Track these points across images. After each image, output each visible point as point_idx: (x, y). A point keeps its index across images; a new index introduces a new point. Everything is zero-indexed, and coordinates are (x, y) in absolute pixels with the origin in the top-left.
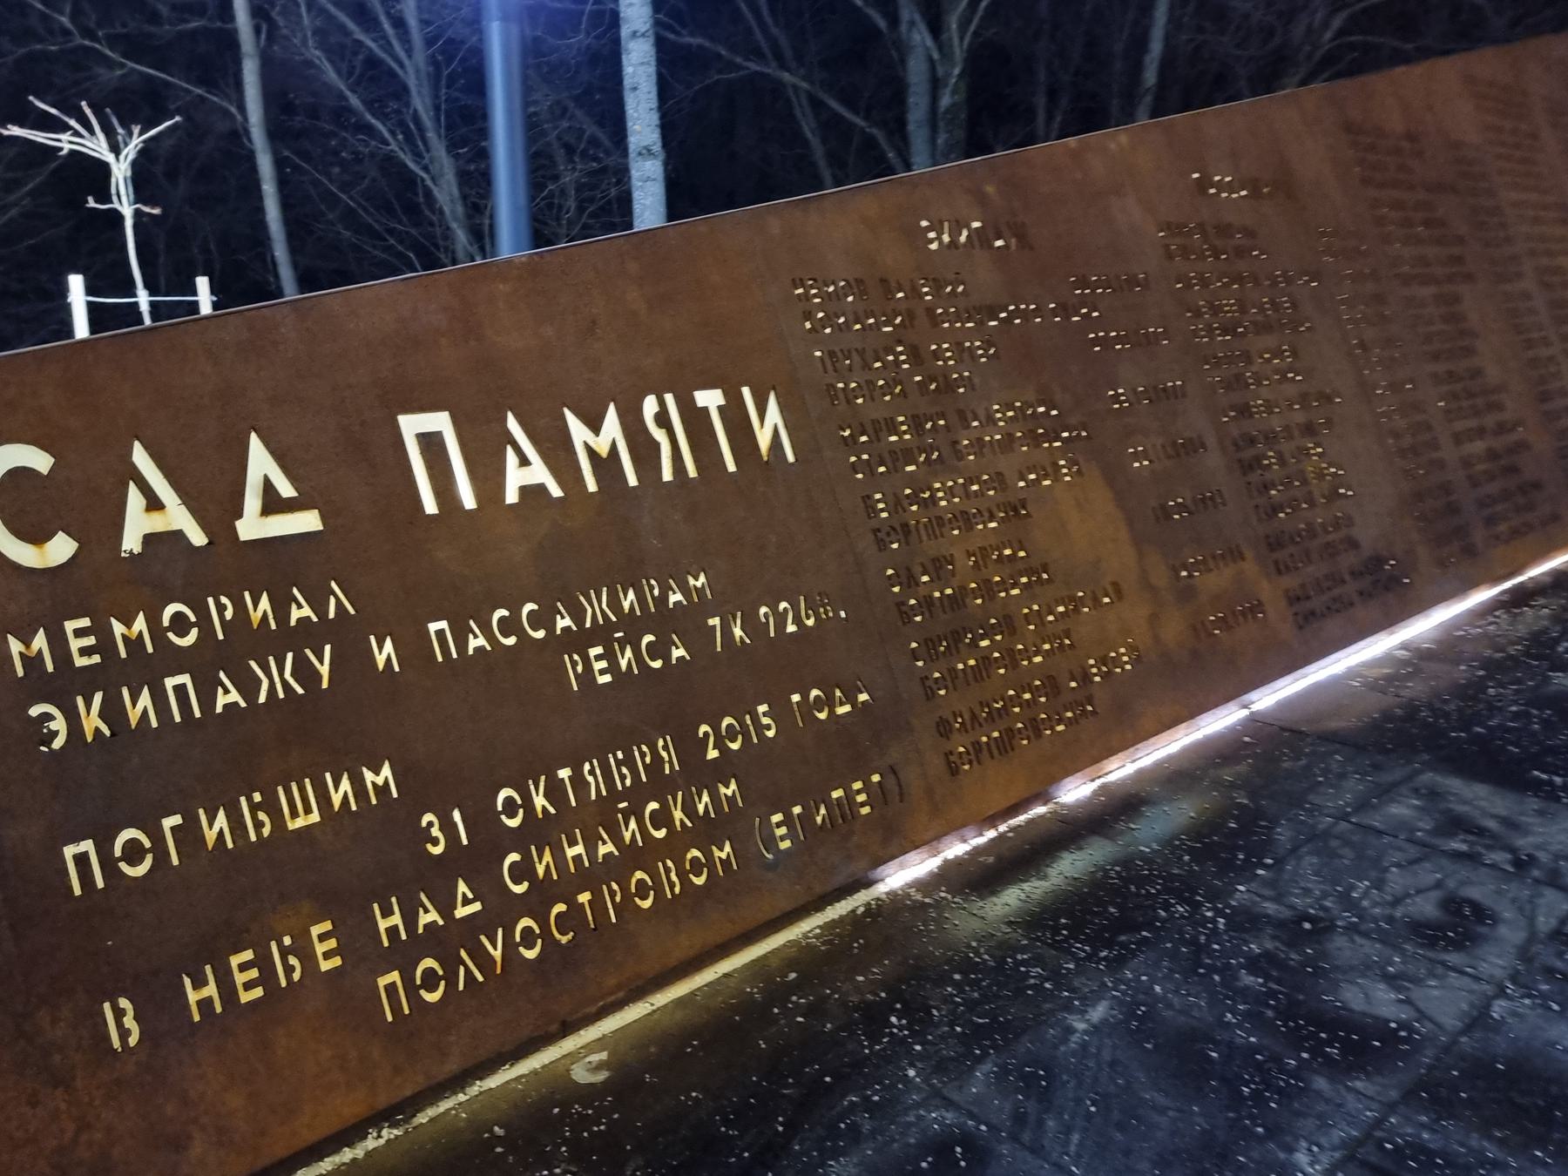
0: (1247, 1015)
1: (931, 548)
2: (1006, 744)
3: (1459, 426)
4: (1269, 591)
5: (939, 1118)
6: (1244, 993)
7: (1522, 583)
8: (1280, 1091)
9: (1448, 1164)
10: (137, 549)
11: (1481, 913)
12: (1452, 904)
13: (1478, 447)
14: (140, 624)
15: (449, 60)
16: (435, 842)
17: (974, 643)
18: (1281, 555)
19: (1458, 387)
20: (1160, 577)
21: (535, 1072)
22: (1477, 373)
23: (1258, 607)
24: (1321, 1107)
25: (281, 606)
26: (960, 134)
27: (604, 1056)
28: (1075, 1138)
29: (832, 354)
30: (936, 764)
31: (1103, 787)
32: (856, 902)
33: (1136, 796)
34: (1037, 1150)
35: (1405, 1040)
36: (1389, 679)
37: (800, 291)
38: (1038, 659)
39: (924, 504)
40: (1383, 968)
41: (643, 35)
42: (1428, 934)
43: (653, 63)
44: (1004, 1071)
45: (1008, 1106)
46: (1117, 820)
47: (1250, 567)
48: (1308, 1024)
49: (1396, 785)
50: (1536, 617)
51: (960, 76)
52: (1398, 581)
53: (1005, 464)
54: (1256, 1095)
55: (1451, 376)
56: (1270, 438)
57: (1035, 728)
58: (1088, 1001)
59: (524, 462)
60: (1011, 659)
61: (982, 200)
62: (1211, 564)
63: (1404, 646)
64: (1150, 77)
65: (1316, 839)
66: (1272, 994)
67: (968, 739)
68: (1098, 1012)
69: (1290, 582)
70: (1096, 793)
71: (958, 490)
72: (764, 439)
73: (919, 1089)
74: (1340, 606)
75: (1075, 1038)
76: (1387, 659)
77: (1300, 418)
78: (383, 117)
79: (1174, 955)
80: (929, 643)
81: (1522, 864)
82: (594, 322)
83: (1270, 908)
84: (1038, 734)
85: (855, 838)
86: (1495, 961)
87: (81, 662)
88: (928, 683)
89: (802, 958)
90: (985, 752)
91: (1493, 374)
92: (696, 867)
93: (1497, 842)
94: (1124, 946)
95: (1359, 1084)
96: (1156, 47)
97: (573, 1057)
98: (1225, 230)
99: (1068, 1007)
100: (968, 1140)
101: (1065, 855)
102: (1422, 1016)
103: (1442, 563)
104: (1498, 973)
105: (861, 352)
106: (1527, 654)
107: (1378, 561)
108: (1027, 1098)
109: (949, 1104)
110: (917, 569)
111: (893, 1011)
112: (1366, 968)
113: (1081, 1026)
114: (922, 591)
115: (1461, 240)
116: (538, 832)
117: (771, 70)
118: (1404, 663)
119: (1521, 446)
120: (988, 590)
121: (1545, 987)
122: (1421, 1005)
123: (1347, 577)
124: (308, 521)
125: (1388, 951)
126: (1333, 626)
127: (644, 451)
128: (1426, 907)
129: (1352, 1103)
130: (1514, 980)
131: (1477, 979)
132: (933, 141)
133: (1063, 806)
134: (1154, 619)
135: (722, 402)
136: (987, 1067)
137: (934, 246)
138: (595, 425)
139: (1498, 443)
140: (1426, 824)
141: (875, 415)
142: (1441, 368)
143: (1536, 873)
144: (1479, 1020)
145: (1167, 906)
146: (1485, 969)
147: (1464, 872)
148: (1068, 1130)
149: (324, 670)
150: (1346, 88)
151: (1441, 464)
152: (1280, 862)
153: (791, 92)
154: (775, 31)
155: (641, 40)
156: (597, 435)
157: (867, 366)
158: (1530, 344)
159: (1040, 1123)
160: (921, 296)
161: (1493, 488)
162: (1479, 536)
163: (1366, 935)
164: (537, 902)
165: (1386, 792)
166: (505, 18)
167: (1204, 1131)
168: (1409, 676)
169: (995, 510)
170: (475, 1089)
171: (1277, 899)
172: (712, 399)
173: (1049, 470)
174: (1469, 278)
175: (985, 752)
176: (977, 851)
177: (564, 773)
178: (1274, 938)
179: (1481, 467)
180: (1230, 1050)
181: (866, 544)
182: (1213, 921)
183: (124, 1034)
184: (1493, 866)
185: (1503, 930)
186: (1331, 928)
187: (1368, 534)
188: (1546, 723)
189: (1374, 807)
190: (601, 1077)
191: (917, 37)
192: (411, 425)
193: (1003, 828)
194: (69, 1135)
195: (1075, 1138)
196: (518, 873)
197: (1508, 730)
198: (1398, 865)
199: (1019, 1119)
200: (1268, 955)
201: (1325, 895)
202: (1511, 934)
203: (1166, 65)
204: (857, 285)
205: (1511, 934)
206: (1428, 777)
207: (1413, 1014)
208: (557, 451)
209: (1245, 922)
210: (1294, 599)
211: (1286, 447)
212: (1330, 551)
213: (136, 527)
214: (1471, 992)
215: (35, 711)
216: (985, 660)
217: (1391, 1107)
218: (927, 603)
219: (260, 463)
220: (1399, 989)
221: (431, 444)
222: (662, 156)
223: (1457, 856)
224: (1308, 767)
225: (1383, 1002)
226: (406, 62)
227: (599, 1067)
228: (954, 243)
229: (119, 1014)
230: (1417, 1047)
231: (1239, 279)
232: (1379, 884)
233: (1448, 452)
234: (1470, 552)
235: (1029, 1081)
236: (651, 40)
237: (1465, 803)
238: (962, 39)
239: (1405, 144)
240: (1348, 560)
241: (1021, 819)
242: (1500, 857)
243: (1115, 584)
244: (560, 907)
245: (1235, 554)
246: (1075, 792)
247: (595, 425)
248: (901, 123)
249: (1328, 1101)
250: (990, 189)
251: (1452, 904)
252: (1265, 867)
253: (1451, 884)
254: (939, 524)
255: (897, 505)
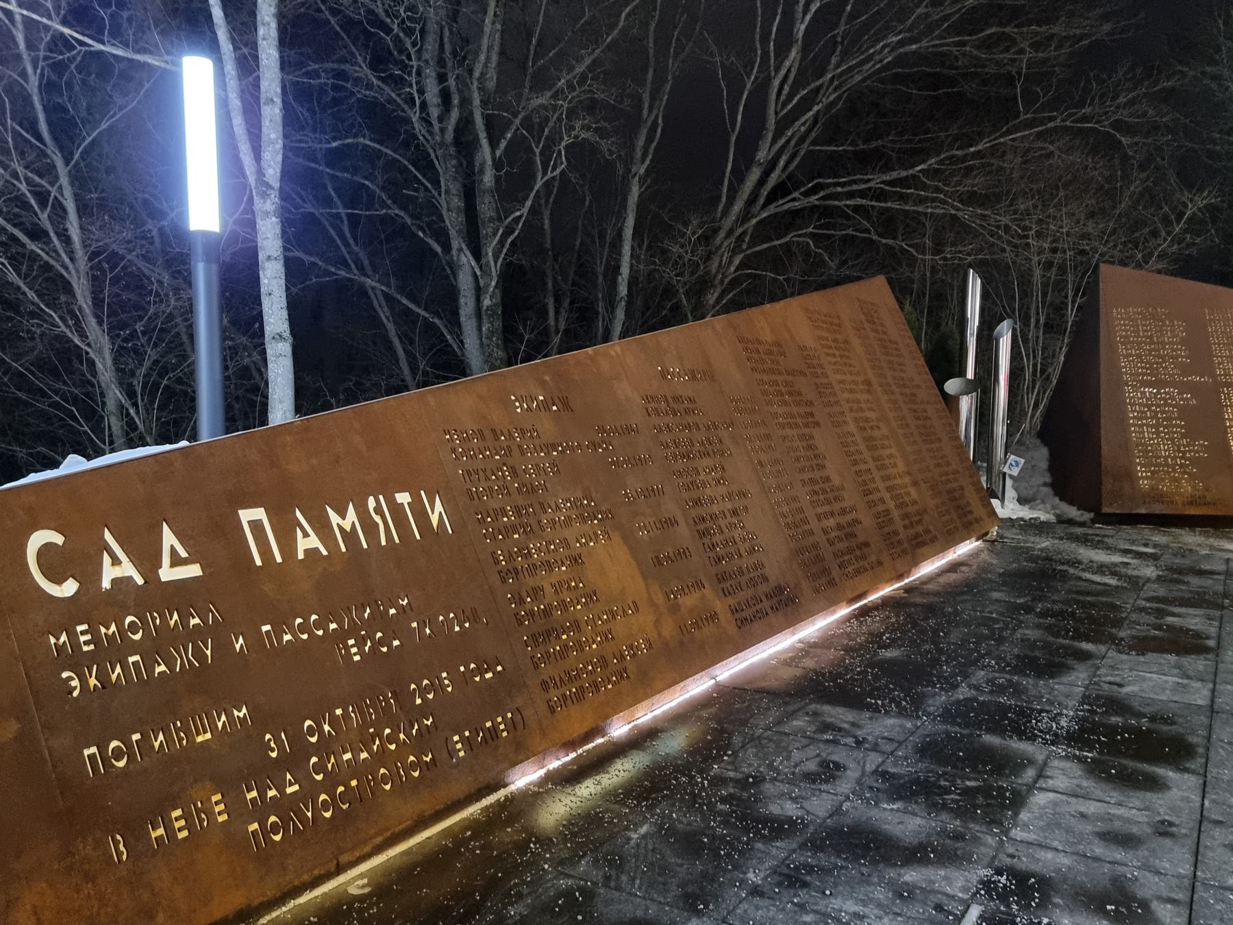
0: (721, 822)
1: (531, 582)
2: (580, 696)
3: (820, 510)
4: (720, 606)
5: (563, 883)
6: (720, 813)
7: (865, 605)
8: (740, 852)
9: (819, 870)
10: (109, 587)
11: (838, 766)
12: (824, 764)
13: (831, 522)
14: (113, 628)
15: (112, 269)
16: (273, 750)
17: (558, 637)
18: (726, 585)
19: (816, 488)
20: (659, 598)
21: (325, 894)
22: (828, 479)
23: (714, 616)
24: (759, 855)
25: (184, 618)
26: (498, 324)
27: (365, 881)
28: (638, 882)
29: (468, 472)
30: (543, 708)
31: (635, 726)
32: (501, 794)
33: (655, 728)
34: (618, 888)
35: (799, 824)
36: (792, 659)
37: (448, 437)
38: (594, 646)
39: (525, 557)
40: (790, 795)
41: (276, 259)
42: (811, 778)
43: (284, 277)
44: (596, 860)
45: (601, 873)
46: (645, 741)
47: (708, 591)
48: (752, 822)
49: (794, 712)
50: (874, 623)
51: (496, 287)
52: (793, 601)
53: (568, 533)
54: (728, 855)
55: (813, 481)
56: (713, 517)
57: (596, 687)
58: (637, 826)
59: (306, 535)
60: (580, 646)
61: (543, 383)
62: (686, 590)
63: (800, 641)
64: (623, 290)
65: (755, 740)
66: (735, 812)
67: (558, 692)
68: (644, 829)
69: (731, 601)
70: (630, 729)
71: (543, 548)
72: (435, 520)
73: (551, 872)
74: (761, 615)
75: (633, 841)
76: (792, 648)
77: (729, 505)
78: (55, 308)
79: (682, 800)
80: (534, 637)
81: (859, 743)
82: (338, 457)
83: (732, 774)
84: (598, 690)
85: (500, 750)
86: (844, 786)
87: (85, 648)
88: (535, 660)
89: (471, 824)
90: (569, 701)
91: (836, 480)
92: (413, 766)
93: (847, 733)
94: (656, 799)
95: (778, 844)
96: (625, 271)
97: (349, 883)
98: (677, 399)
99: (627, 828)
100: (583, 890)
101: (618, 760)
102: (808, 813)
103: (817, 590)
104: (846, 791)
105: (484, 471)
106: (867, 641)
107: (780, 589)
108: (610, 869)
109: (568, 876)
110: (524, 594)
111: (531, 842)
112: (782, 795)
113: (636, 836)
114: (528, 607)
115: (811, 404)
116: (326, 747)
117: (356, 276)
118: (802, 650)
119: (857, 522)
120: (563, 606)
121: (868, 795)
122: (808, 808)
123: (764, 598)
124: (194, 570)
125: (792, 787)
126: (757, 626)
127: (370, 528)
128: (812, 766)
129: (774, 851)
130: (853, 793)
131: (836, 795)
132: (479, 329)
133: (613, 738)
134: (657, 623)
135: (410, 500)
136: (587, 859)
137: (519, 410)
138: (343, 515)
139: (843, 520)
140: (813, 728)
141: (495, 506)
142: (806, 476)
143: (867, 746)
144: (837, 811)
145: (676, 779)
146: (840, 790)
147: (831, 748)
148: (634, 879)
149: (209, 652)
150: (737, 317)
151: (811, 533)
152: (735, 754)
153: (370, 292)
154: (356, 249)
155: (274, 262)
156: (344, 519)
157: (488, 479)
158: (855, 463)
159: (618, 878)
160: (514, 439)
161: (842, 546)
162: (835, 572)
163: (782, 781)
164: (329, 784)
165: (792, 715)
166: (208, 261)
167: (702, 871)
168: (803, 657)
169: (564, 560)
170: (292, 904)
171: (735, 770)
172: (403, 498)
173: (593, 537)
174: (817, 424)
175: (569, 701)
176: (564, 765)
177: (339, 712)
178: (734, 787)
179: (834, 534)
180: (713, 838)
181: (495, 579)
182: (702, 783)
183: (119, 854)
184: (846, 745)
185: (849, 772)
186: (764, 780)
187: (774, 572)
188: (876, 677)
189: (785, 723)
190: (367, 890)
191: (464, 259)
192: (247, 515)
193: (580, 751)
194: (95, 910)
195: (638, 882)
196: (319, 768)
197: (856, 680)
198: (797, 749)
199: (607, 878)
200: (731, 796)
201: (760, 766)
202: (853, 774)
203: (633, 282)
204: (481, 434)
205: (853, 774)
206: (813, 707)
207: (804, 812)
208: (323, 528)
209: (719, 781)
210: (734, 611)
211: (722, 523)
212: (753, 583)
213: (108, 574)
214: (833, 800)
215: (65, 675)
216: (565, 647)
217: (794, 851)
218: (531, 614)
219: (169, 538)
220: (797, 803)
221: (256, 526)
222: (290, 340)
223: (828, 741)
224: (750, 705)
225: (791, 809)
226: (71, 266)
227: (363, 886)
228: (529, 409)
229: (116, 843)
230: (806, 826)
231: (688, 426)
232: (788, 758)
233: (814, 525)
234: (832, 583)
235: (611, 864)
236: (282, 262)
237: (832, 717)
238: (496, 262)
239: (776, 349)
240: (763, 588)
241: (590, 746)
242: (850, 741)
243: (634, 602)
244: (341, 789)
245: (699, 585)
246: (619, 729)
247: (343, 515)
248: (455, 313)
249: (763, 852)
250: (547, 378)
251: (824, 764)
252: (728, 756)
253: (824, 755)
254: (533, 569)
255: (510, 557)
